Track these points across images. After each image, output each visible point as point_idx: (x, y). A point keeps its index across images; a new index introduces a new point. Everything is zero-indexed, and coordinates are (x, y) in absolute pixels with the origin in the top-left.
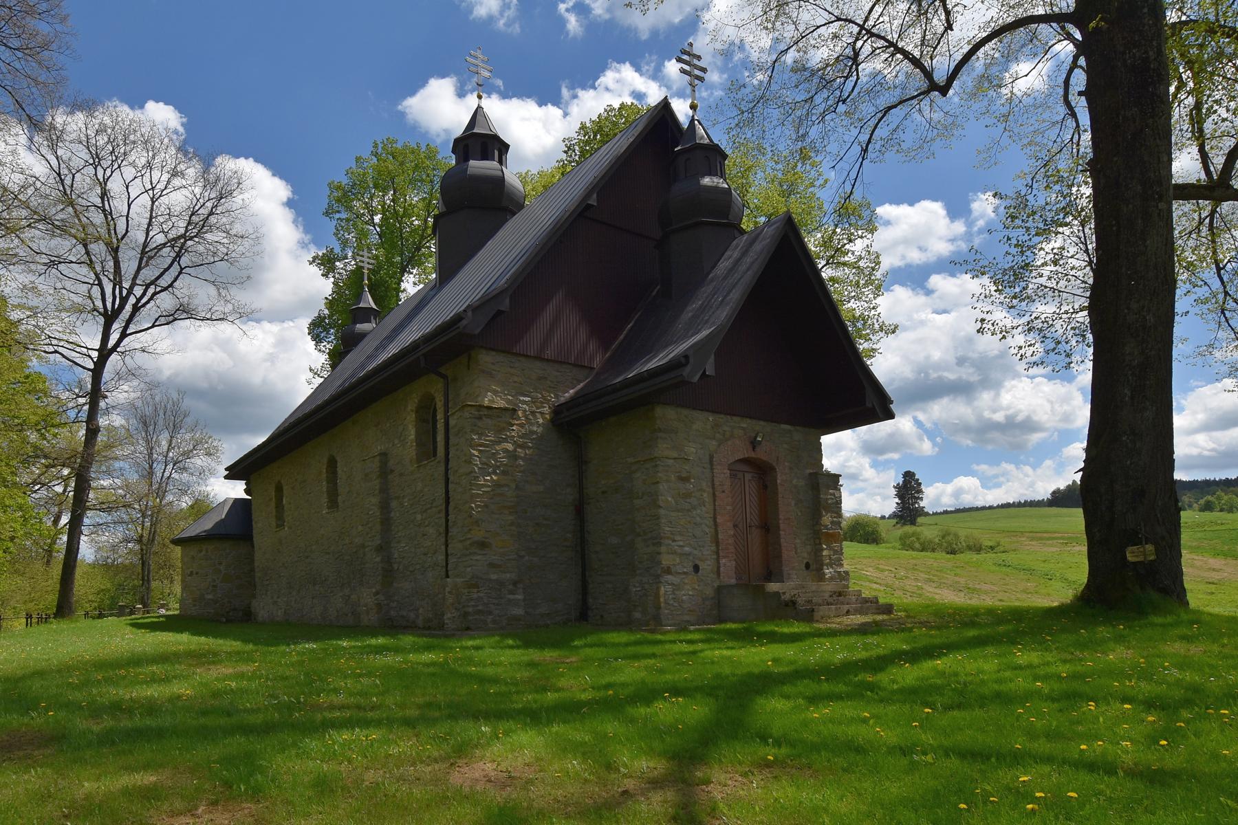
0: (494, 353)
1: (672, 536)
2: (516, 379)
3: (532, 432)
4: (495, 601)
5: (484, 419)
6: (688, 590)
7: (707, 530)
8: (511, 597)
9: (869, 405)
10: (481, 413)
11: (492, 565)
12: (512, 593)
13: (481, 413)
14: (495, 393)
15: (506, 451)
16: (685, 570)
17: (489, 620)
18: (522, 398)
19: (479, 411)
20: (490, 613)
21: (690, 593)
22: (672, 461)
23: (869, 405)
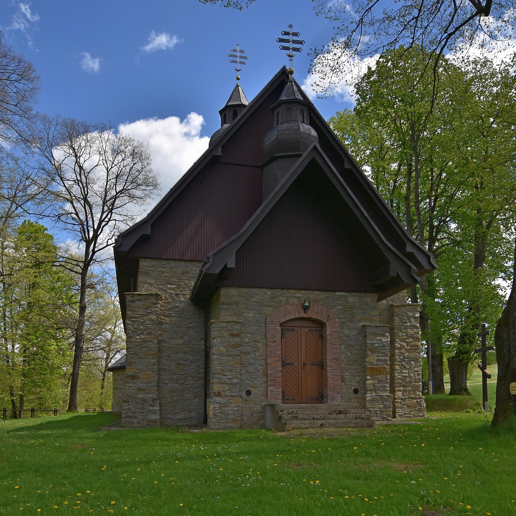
0: (150, 260)
1: (223, 372)
2: (166, 274)
3: (176, 307)
4: (140, 411)
5: (136, 301)
6: (234, 407)
7: (259, 368)
8: (151, 408)
9: (393, 274)
10: (134, 298)
11: (140, 389)
12: (151, 406)
13: (134, 298)
14: (150, 284)
15: (150, 320)
16: (233, 394)
17: (135, 422)
18: (169, 286)
19: (132, 297)
20: (136, 417)
21: (235, 409)
22: (226, 324)
23: (393, 274)
